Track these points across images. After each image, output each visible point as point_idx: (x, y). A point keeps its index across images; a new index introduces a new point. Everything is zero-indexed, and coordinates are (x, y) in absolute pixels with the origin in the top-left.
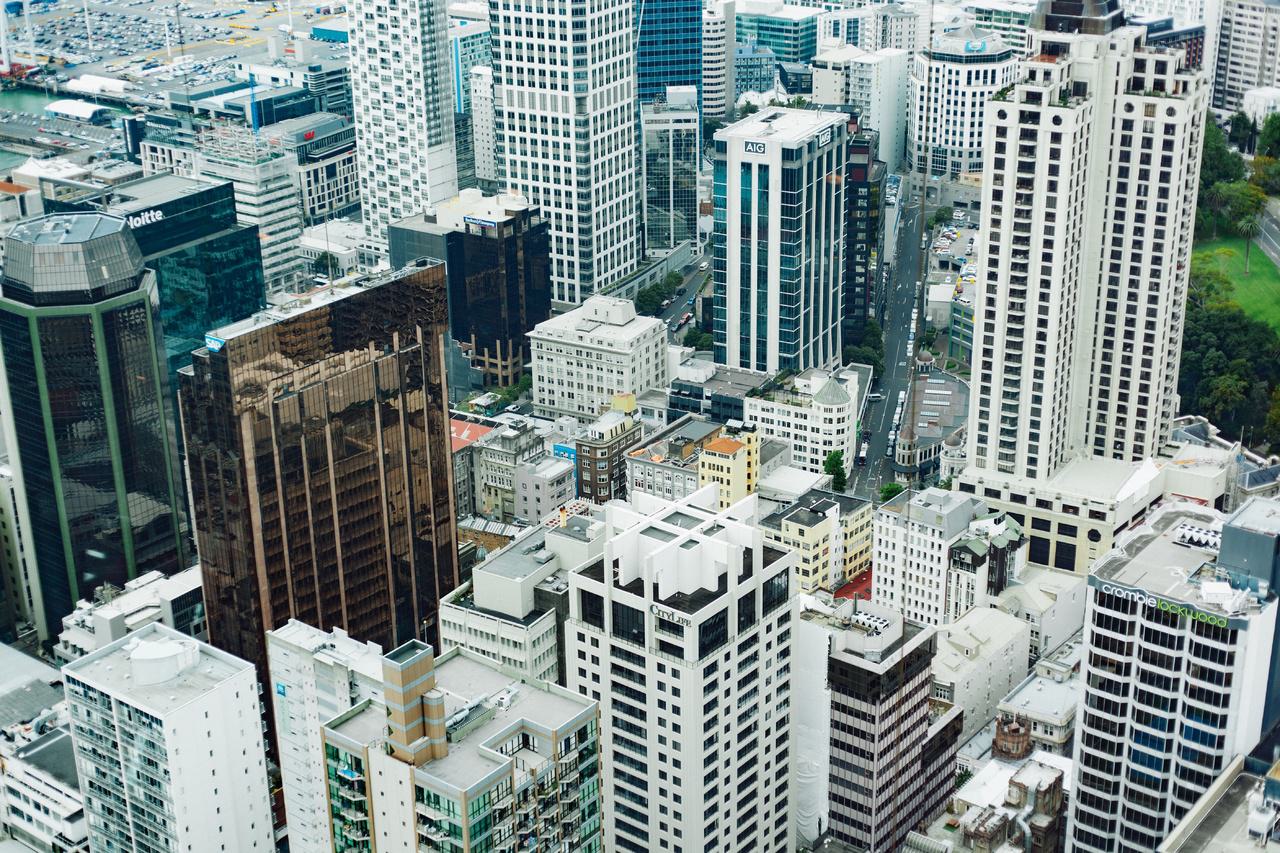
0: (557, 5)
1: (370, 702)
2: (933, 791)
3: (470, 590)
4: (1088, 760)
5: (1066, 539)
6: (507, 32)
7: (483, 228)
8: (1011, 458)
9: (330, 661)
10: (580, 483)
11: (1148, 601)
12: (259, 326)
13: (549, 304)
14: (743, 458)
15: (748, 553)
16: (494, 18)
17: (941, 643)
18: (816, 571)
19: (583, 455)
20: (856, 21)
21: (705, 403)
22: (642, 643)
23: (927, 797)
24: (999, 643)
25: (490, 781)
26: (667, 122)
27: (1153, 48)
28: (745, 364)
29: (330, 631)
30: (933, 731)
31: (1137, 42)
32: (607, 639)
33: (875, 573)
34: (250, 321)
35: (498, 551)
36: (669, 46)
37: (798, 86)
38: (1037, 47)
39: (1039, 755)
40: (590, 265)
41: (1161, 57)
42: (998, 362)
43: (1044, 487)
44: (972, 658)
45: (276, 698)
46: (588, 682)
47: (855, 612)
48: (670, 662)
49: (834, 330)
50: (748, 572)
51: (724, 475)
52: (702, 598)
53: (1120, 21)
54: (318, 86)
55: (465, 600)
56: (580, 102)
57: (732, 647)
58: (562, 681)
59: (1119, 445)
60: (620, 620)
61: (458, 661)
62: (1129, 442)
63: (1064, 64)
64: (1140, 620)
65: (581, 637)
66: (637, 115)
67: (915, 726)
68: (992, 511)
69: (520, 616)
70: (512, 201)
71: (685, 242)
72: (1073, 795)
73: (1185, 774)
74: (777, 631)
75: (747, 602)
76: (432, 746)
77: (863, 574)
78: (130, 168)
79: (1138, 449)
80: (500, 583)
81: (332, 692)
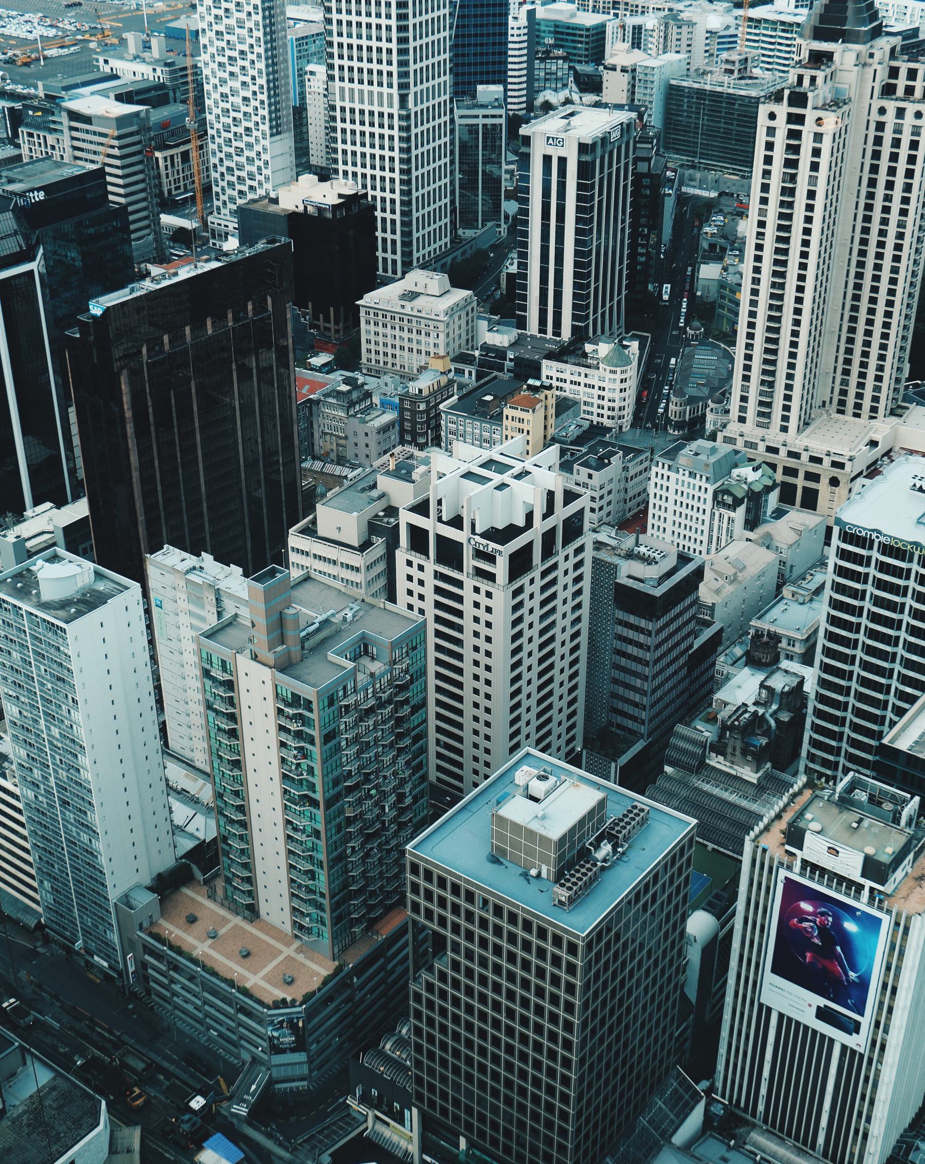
0: (333, 5)
1: (236, 615)
2: (696, 691)
3: (314, 522)
4: (826, 668)
5: (811, 485)
6: (340, 34)
7: (319, 209)
8: (768, 415)
9: (199, 581)
10: (402, 432)
11: (882, 539)
12: (135, 295)
13: (376, 276)
14: (540, 412)
15: (551, 495)
16: (329, 21)
17: (708, 574)
18: (601, 509)
19: (406, 404)
20: (640, 27)
21: (508, 364)
22: (460, 569)
23: (691, 696)
24: (752, 570)
25: (337, 683)
26: (477, 117)
27: (906, 57)
28: (543, 330)
29: (198, 555)
30: (697, 644)
31: (893, 50)
32: (431, 566)
33: (651, 511)
34: (127, 290)
35: (337, 489)
36: (477, 51)
37: (591, 85)
38: (805, 55)
39: (785, 664)
40: (411, 243)
41: (912, 65)
42: (760, 333)
43: (796, 440)
44: (732, 582)
45: (155, 610)
46: (414, 601)
47: (637, 544)
48: (484, 586)
49: (619, 302)
50: (549, 511)
51: (525, 426)
52: (512, 532)
53: (877, 32)
54: (172, 80)
55: (310, 531)
56: (403, 99)
57: (536, 574)
58: (392, 598)
59: (858, 406)
61: (308, 586)
62: (867, 403)
63: (828, 71)
64: (875, 554)
65: (409, 563)
66: (452, 111)
67: (684, 639)
68: (751, 460)
69: (356, 544)
70: (348, 187)
71: (489, 224)
72: (812, 696)
73: (905, 680)
74: (573, 561)
75: (549, 537)
77: (640, 512)
78: (10, 151)
79: (874, 410)
80: (338, 518)
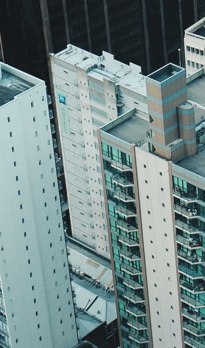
9: (100, 78)
45: (59, 106)
60: (167, 78)
76: (185, 146)
81: (103, 103)
